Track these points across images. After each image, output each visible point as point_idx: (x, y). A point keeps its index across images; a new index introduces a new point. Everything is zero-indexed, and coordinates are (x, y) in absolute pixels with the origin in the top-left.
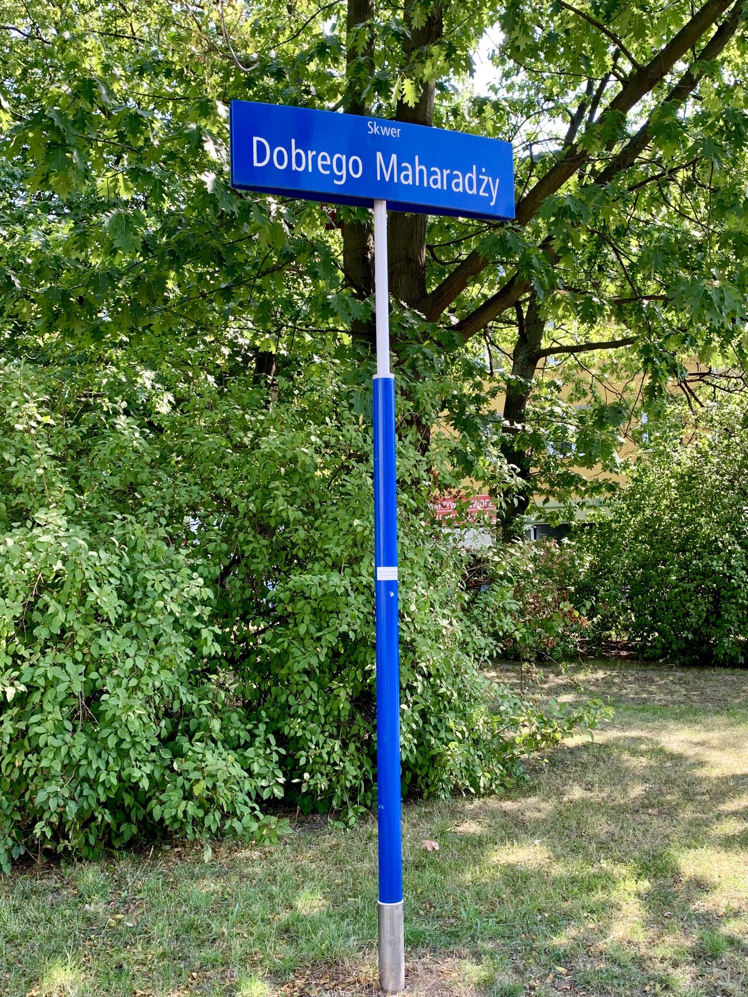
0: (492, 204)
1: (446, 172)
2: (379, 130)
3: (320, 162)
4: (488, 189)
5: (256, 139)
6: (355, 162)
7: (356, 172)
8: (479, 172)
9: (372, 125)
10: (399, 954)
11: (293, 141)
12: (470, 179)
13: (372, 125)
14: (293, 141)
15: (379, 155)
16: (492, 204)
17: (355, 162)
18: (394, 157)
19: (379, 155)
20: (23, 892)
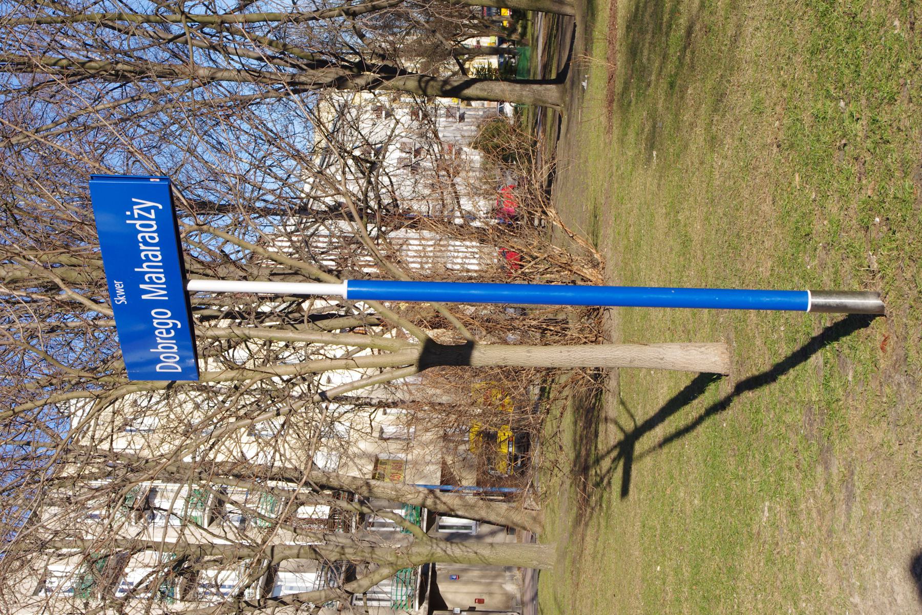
0: (161, 207)
1: (142, 247)
2: (121, 296)
3: (165, 335)
4: (147, 210)
5: (158, 370)
6: (156, 313)
7: (167, 314)
8: (132, 217)
9: (119, 301)
10: (551, 332)
11: (136, 270)
12: (141, 226)
13: (119, 301)
14: (136, 270)
15: (144, 297)
16: (161, 207)
17: (156, 313)
18: (142, 286)
19: (144, 297)
20: (136, 401)
